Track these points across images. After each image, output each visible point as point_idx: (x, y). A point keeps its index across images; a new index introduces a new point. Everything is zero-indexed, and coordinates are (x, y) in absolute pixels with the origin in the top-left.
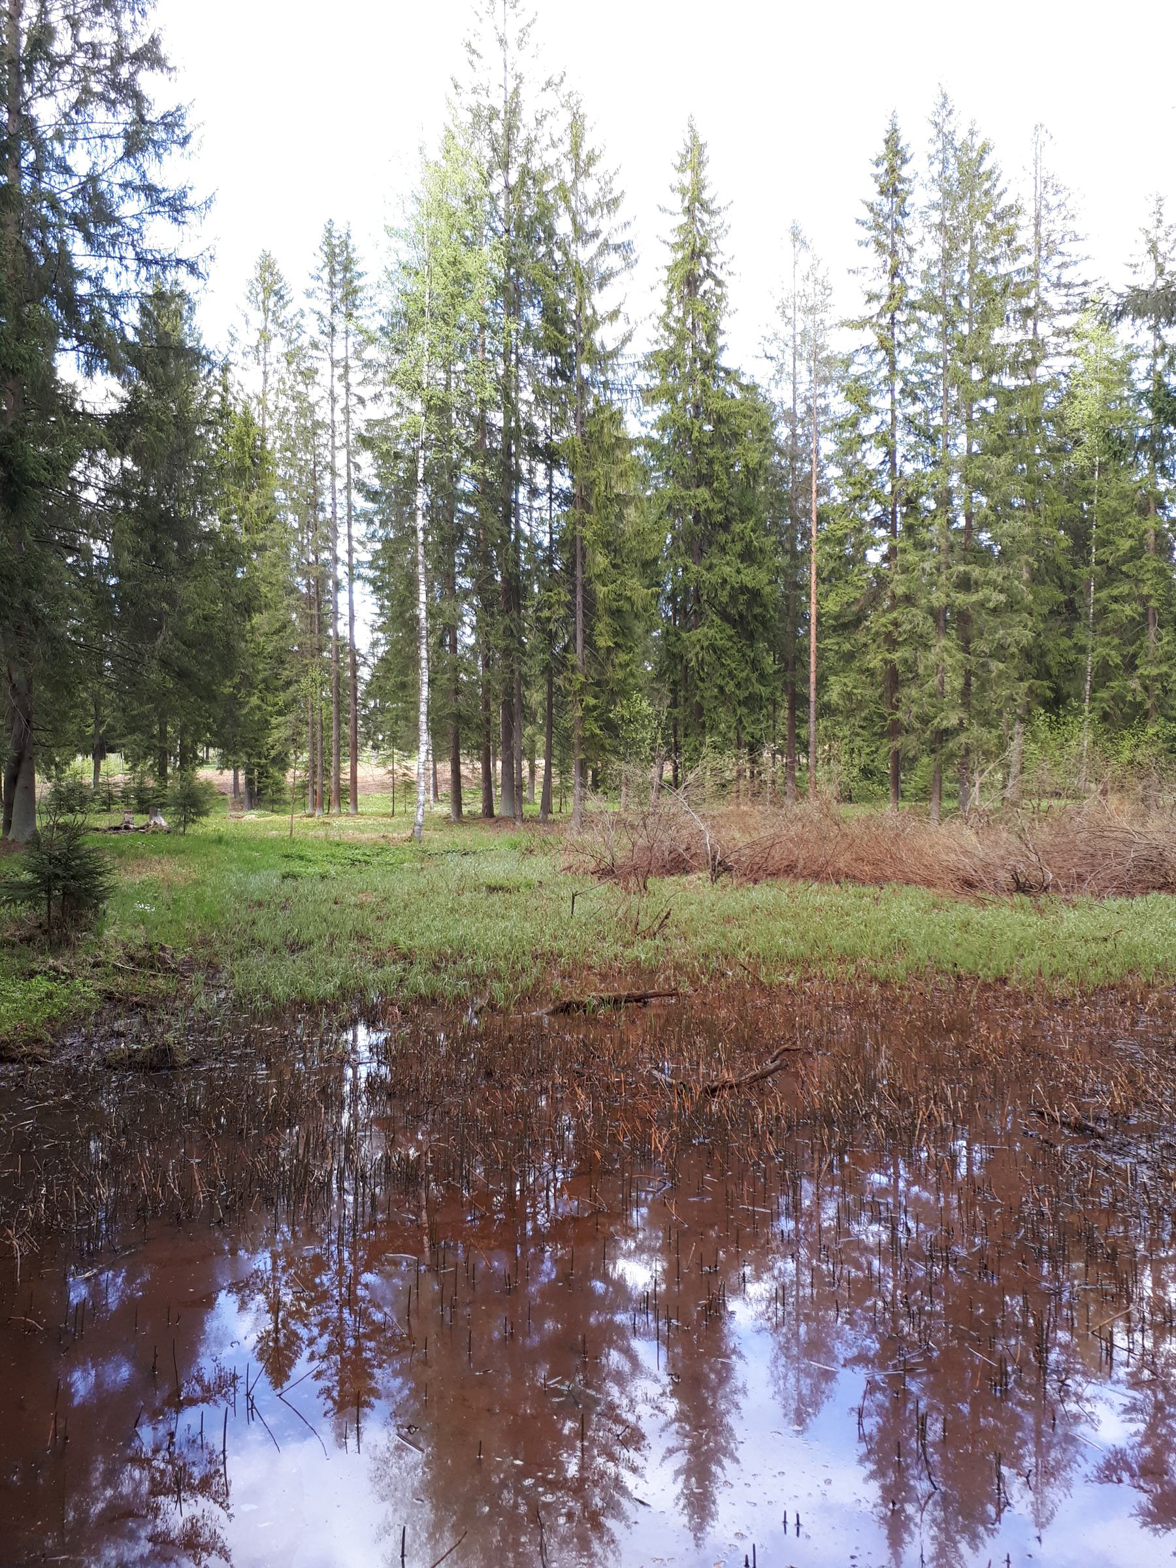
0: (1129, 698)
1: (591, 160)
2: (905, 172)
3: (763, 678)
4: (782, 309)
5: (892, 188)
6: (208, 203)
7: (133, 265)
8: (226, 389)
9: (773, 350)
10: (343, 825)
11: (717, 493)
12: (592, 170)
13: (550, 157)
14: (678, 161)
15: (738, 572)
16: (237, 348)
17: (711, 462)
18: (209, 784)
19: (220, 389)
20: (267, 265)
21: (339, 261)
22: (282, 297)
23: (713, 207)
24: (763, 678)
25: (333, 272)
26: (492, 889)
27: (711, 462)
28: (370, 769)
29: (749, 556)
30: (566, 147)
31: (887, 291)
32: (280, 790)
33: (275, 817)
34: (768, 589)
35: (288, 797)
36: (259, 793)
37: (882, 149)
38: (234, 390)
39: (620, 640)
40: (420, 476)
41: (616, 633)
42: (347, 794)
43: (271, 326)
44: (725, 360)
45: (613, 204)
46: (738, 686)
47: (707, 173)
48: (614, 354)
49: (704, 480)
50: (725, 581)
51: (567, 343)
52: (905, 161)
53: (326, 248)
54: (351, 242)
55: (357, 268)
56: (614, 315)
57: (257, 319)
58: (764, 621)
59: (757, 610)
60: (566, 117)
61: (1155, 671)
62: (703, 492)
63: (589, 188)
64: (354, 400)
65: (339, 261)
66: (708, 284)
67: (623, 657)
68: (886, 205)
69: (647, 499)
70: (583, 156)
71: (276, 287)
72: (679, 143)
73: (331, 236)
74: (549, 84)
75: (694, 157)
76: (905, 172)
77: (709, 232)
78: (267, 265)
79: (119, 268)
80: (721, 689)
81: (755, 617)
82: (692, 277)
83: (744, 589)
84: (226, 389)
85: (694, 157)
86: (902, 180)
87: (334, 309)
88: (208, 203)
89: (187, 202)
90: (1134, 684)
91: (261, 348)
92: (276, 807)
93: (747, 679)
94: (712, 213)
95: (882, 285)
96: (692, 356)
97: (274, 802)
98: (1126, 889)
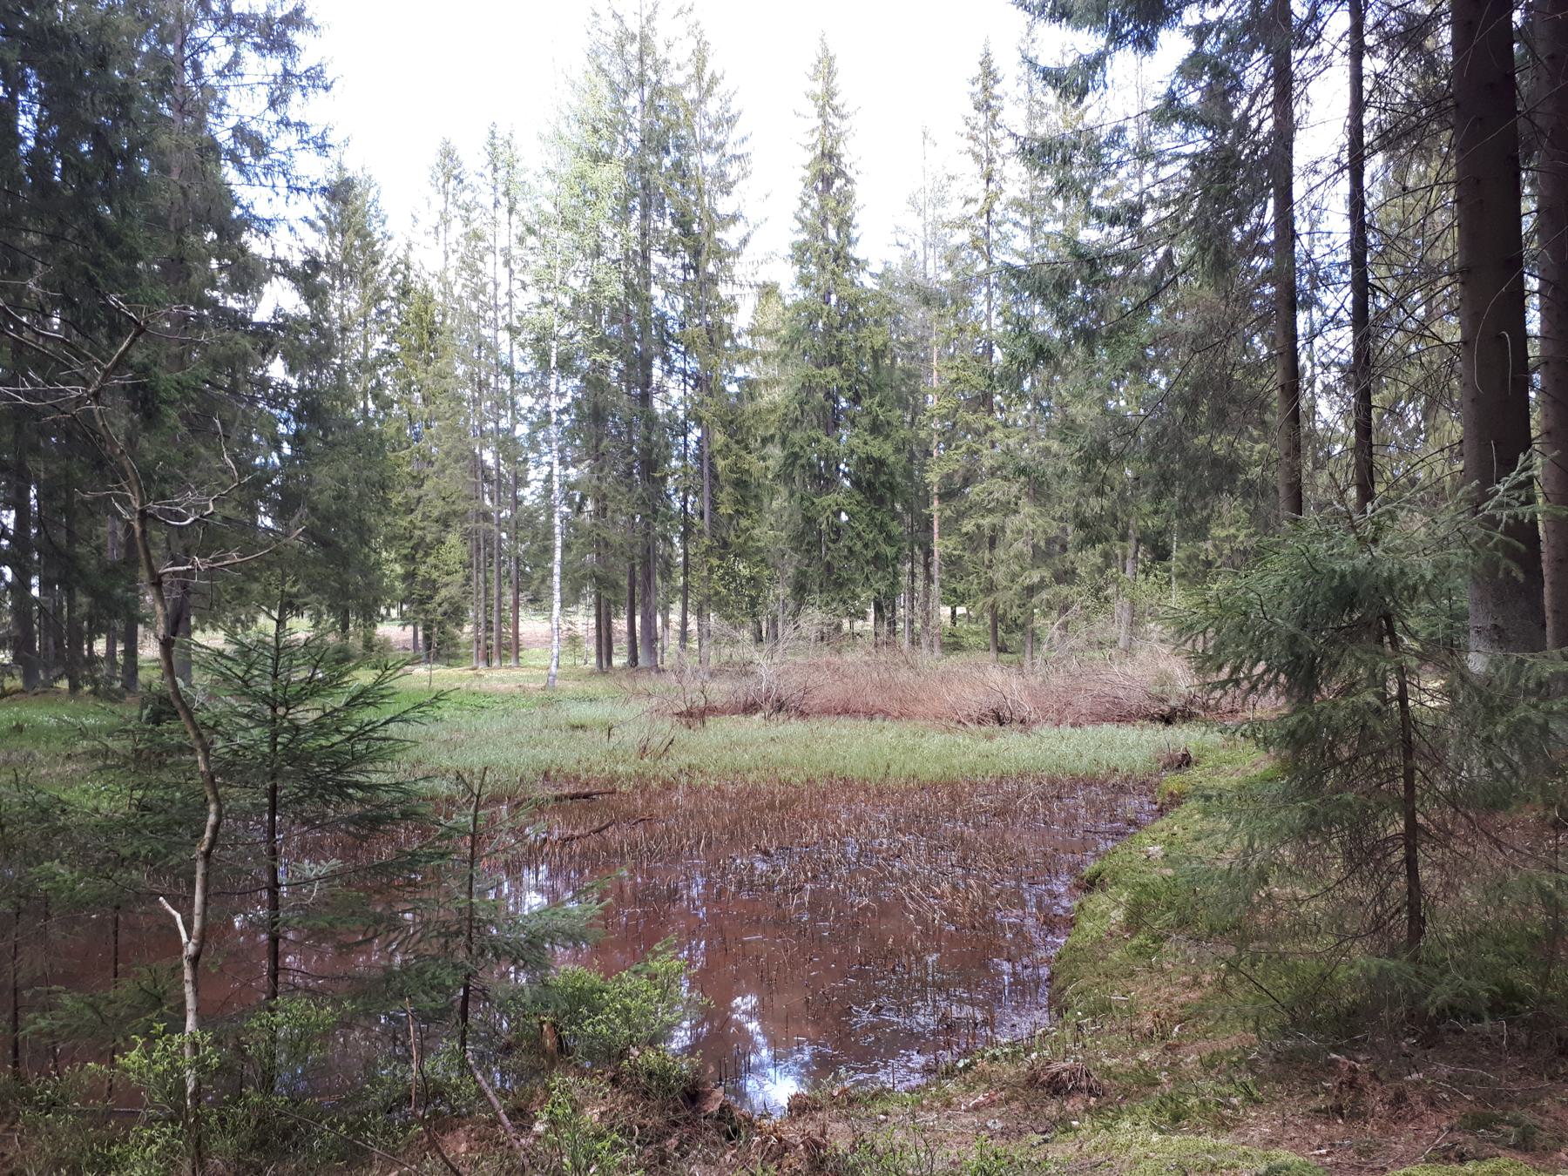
0: (1202, 557)
1: (714, 81)
2: (997, 90)
3: (889, 539)
4: (912, 202)
5: (985, 105)
6: (347, 142)
7: (283, 191)
8: (408, 268)
9: (904, 240)
10: (499, 678)
11: (846, 373)
12: (716, 90)
13: (679, 78)
14: (811, 71)
15: (866, 443)
16: (421, 227)
17: (840, 344)
18: (387, 640)
19: (402, 267)
20: (448, 154)
21: (500, 157)
22: (461, 181)
23: (844, 111)
24: (889, 539)
25: (496, 170)
26: (575, 727)
27: (840, 344)
28: (531, 626)
29: (876, 428)
30: (691, 70)
31: (982, 196)
32: (456, 645)
33: (450, 671)
34: (892, 459)
35: (462, 651)
36: (437, 648)
37: (978, 71)
38: (417, 267)
39: (741, 508)
40: (553, 364)
41: (737, 502)
42: (511, 648)
43: (450, 207)
44: (856, 252)
45: (731, 121)
46: (866, 546)
47: (839, 82)
48: (736, 253)
49: (835, 360)
50: (852, 451)
51: (698, 243)
52: (997, 82)
53: (489, 149)
54: (513, 142)
55: (518, 166)
56: (734, 218)
57: (439, 202)
58: (892, 488)
59: (884, 478)
60: (692, 44)
61: (1224, 534)
62: (833, 371)
63: (712, 107)
64: (516, 285)
65: (500, 157)
66: (838, 183)
67: (744, 523)
68: (981, 119)
69: (765, 378)
70: (706, 78)
71: (455, 172)
72: (809, 57)
73: (494, 137)
74: (680, 12)
75: (826, 68)
76: (997, 90)
77: (840, 135)
78: (448, 154)
79: (273, 195)
80: (850, 549)
81: (882, 484)
82: (828, 173)
83: (869, 459)
84: (408, 268)
85: (826, 68)
86: (997, 98)
87: (496, 204)
88: (347, 142)
89: (328, 141)
90: (1208, 545)
91: (441, 229)
92: (452, 661)
93: (875, 540)
94: (842, 117)
95: (978, 189)
96: (827, 248)
97: (449, 657)
98: (1100, 718)
